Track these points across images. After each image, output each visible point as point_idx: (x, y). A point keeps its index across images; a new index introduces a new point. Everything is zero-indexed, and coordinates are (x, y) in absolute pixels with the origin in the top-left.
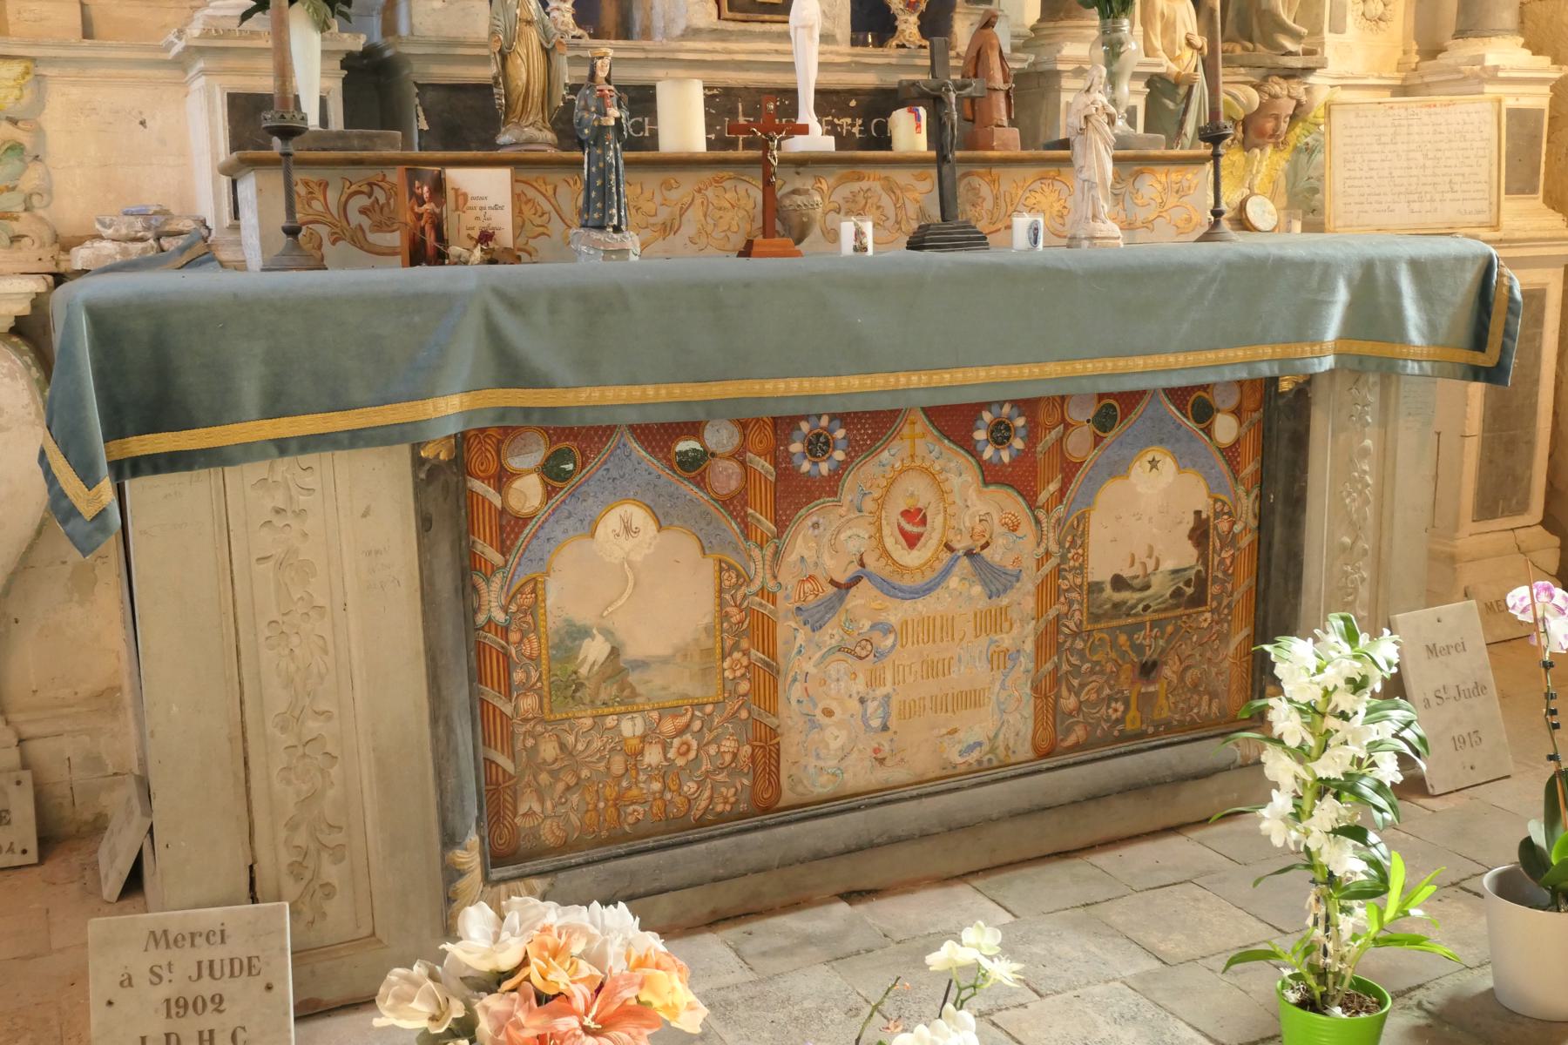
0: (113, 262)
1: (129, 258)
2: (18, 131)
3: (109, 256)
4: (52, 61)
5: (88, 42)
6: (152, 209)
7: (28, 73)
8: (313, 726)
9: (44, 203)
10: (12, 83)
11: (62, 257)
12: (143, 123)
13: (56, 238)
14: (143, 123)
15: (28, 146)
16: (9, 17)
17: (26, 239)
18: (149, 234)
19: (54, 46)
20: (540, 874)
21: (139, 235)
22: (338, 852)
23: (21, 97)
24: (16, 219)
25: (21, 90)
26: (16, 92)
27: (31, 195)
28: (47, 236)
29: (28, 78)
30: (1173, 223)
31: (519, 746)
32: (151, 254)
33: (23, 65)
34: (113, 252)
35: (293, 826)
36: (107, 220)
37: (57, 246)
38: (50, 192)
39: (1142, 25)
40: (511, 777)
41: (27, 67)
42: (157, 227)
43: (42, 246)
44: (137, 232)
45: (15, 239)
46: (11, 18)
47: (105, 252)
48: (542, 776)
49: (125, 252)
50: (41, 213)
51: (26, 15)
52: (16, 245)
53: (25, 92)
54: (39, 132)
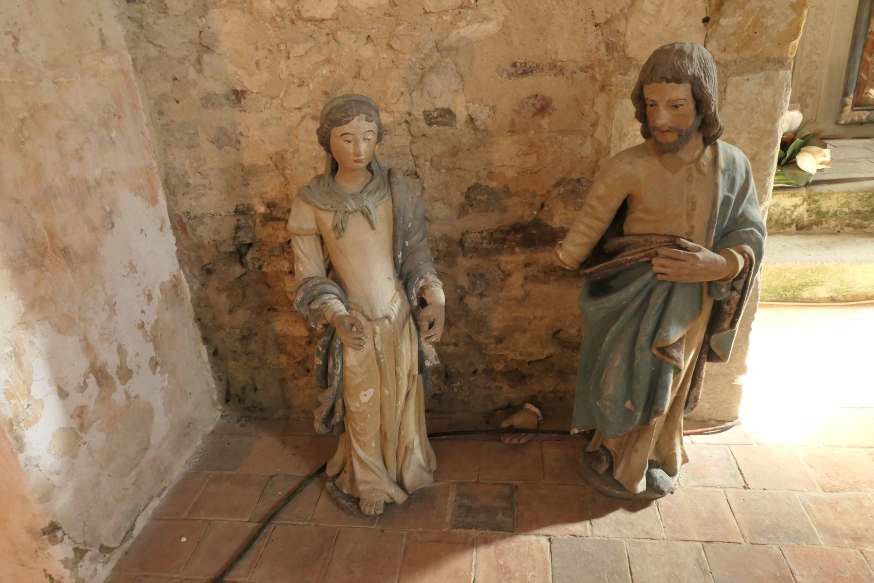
8: (815, 58)
14: (110, 476)
20: (868, 110)
22: (812, 95)
30: (490, 4)
31: (870, 72)
35: (802, 86)
39: (470, 528)
40: (865, 81)
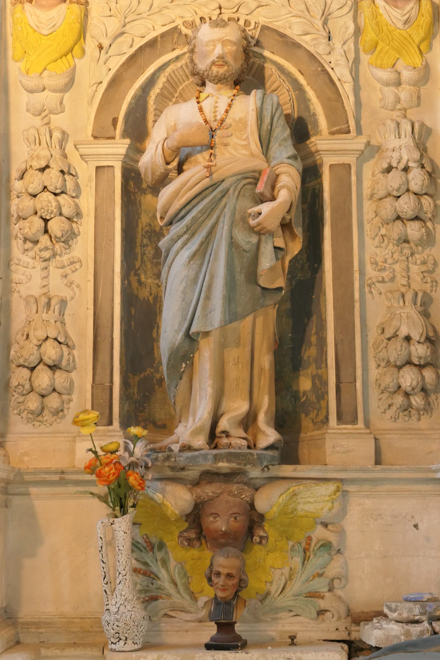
0: (398, 642)
1: (410, 639)
2: (328, 533)
3: (396, 637)
4: (353, 481)
5: (379, 467)
6: (427, 597)
7: (338, 491)
9: (342, 585)
10: (328, 498)
11: (353, 628)
12: (416, 526)
13: (349, 613)
14: (416, 526)
15: (335, 543)
16: (327, 451)
17: (328, 613)
18: (424, 618)
19: (357, 471)
21: (416, 618)
23: (332, 508)
24: (323, 598)
25: (333, 503)
26: (329, 505)
27: (332, 580)
28: (343, 611)
29: (338, 494)
32: (427, 636)
33: (336, 485)
34: (398, 633)
36: (393, 605)
37: (349, 619)
38: (346, 578)
41: (338, 487)
42: (430, 613)
43: (339, 618)
44: (415, 615)
45: (321, 612)
46: (328, 451)
47: (393, 633)
48: (35, 405)
49: (407, 633)
50: (339, 592)
51: (338, 449)
52: (321, 617)
53: (335, 504)
54: (342, 533)
